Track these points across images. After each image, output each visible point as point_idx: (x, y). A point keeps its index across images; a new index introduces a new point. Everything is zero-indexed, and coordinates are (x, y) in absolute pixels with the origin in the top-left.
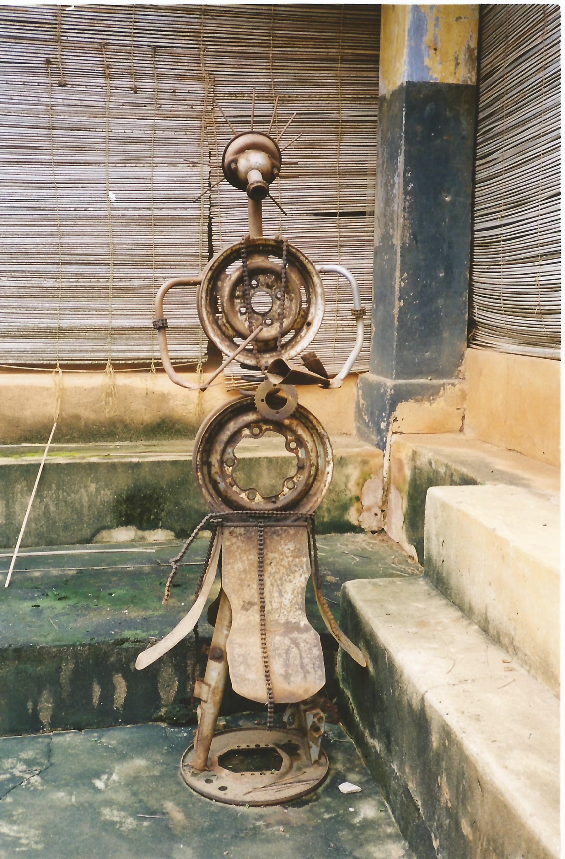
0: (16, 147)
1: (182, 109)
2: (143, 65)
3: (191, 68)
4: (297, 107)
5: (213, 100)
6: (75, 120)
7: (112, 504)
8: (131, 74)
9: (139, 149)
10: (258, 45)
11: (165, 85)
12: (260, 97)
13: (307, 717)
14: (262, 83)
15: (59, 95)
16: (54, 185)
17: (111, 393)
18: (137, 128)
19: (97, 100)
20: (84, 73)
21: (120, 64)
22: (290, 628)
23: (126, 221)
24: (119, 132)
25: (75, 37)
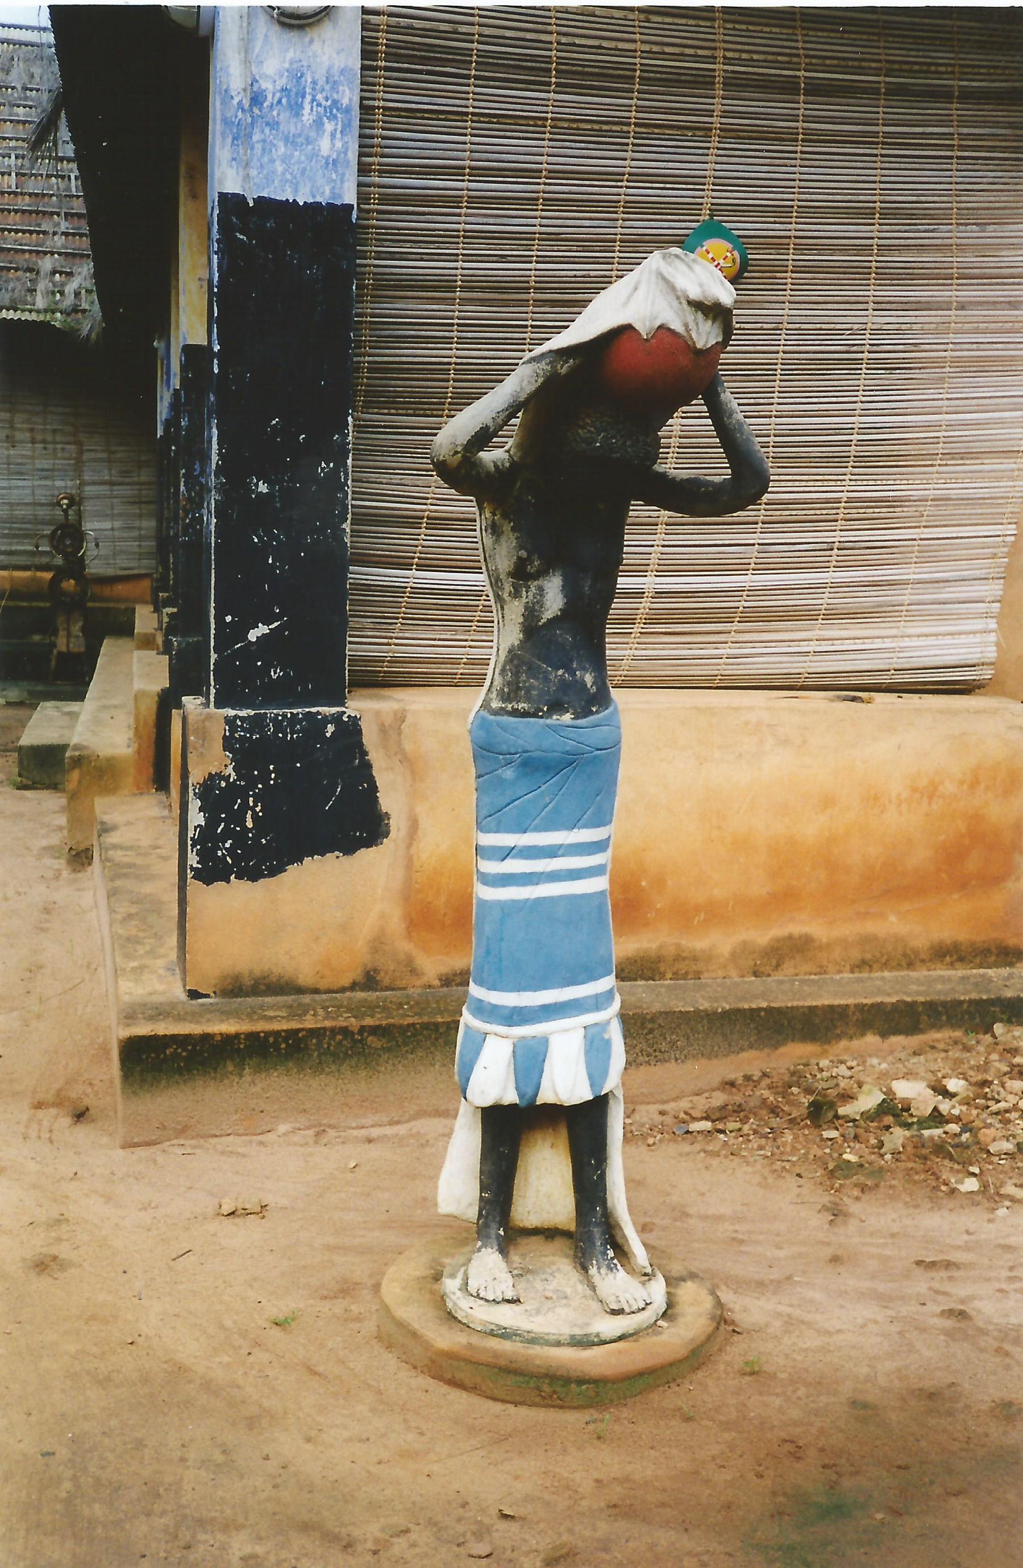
0: (972, 499)
1: (67, 455)
2: (49, 438)
3: (71, 439)
4: (119, 455)
5: (81, 452)
6: (19, 461)
7: (275, 1074)
8: (44, 441)
9: (48, 474)
10: (995, 168)
11: (59, 446)
12: (102, 451)
13: (586, 1411)
14: (888, 306)
15: (12, 452)
16: (10, 488)
17: (34, 579)
18: (46, 464)
19: (29, 453)
20: (22, 442)
21: (39, 437)
22: (77, 637)
23: (42, 505)
24: (39, 466)
25: (19, 426)
